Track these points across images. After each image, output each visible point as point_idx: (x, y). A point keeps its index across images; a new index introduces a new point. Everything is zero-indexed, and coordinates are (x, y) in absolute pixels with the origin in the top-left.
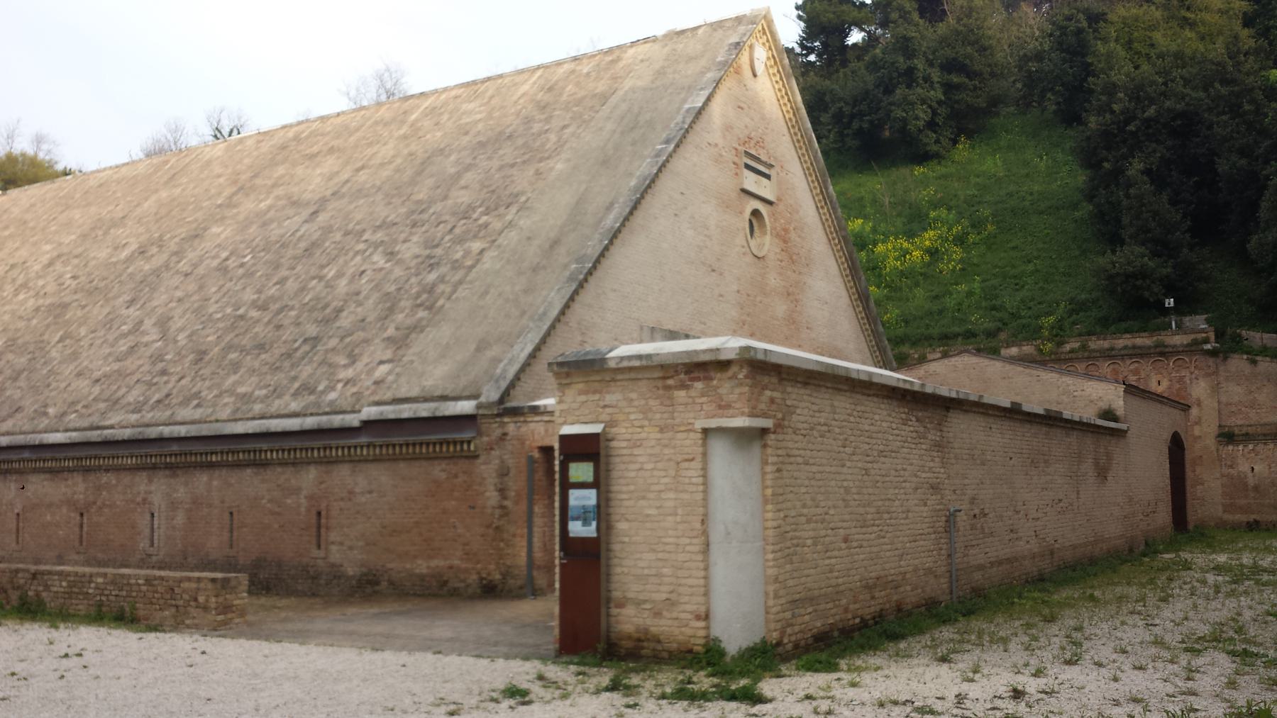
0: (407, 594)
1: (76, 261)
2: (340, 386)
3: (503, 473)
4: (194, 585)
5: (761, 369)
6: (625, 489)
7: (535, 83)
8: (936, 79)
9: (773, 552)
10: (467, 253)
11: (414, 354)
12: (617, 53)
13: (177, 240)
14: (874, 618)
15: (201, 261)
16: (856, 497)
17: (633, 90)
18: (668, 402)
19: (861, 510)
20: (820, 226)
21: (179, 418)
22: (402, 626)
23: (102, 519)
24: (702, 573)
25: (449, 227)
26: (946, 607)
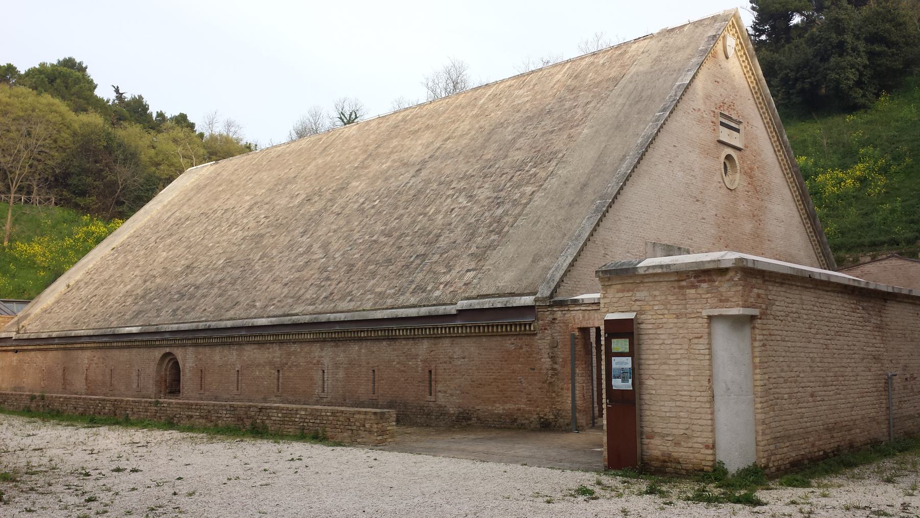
0: (490, 427)
1: (267, 206)
2: (442, 286)
3: (554, 346)
4: (362, 416)
5: (750, 274)
6: (651, 357)
7: (565, 73)
8: (862, 49)
9: (761, 403)
10: (523, 195)
11: (490, 265)
12: (624, 48)
13: (330, 191)
14: (833, 452)
15: (347, 205)
16: (819, 364)
17: (637, 74)
18: (681, 298)
19: (823, 374)
20: (778, 165)
21: (339, 309)
22: (493, 447)
23: (291, 374)
24: (710, 417)
25: (509, 177)
26: (886, 445)
